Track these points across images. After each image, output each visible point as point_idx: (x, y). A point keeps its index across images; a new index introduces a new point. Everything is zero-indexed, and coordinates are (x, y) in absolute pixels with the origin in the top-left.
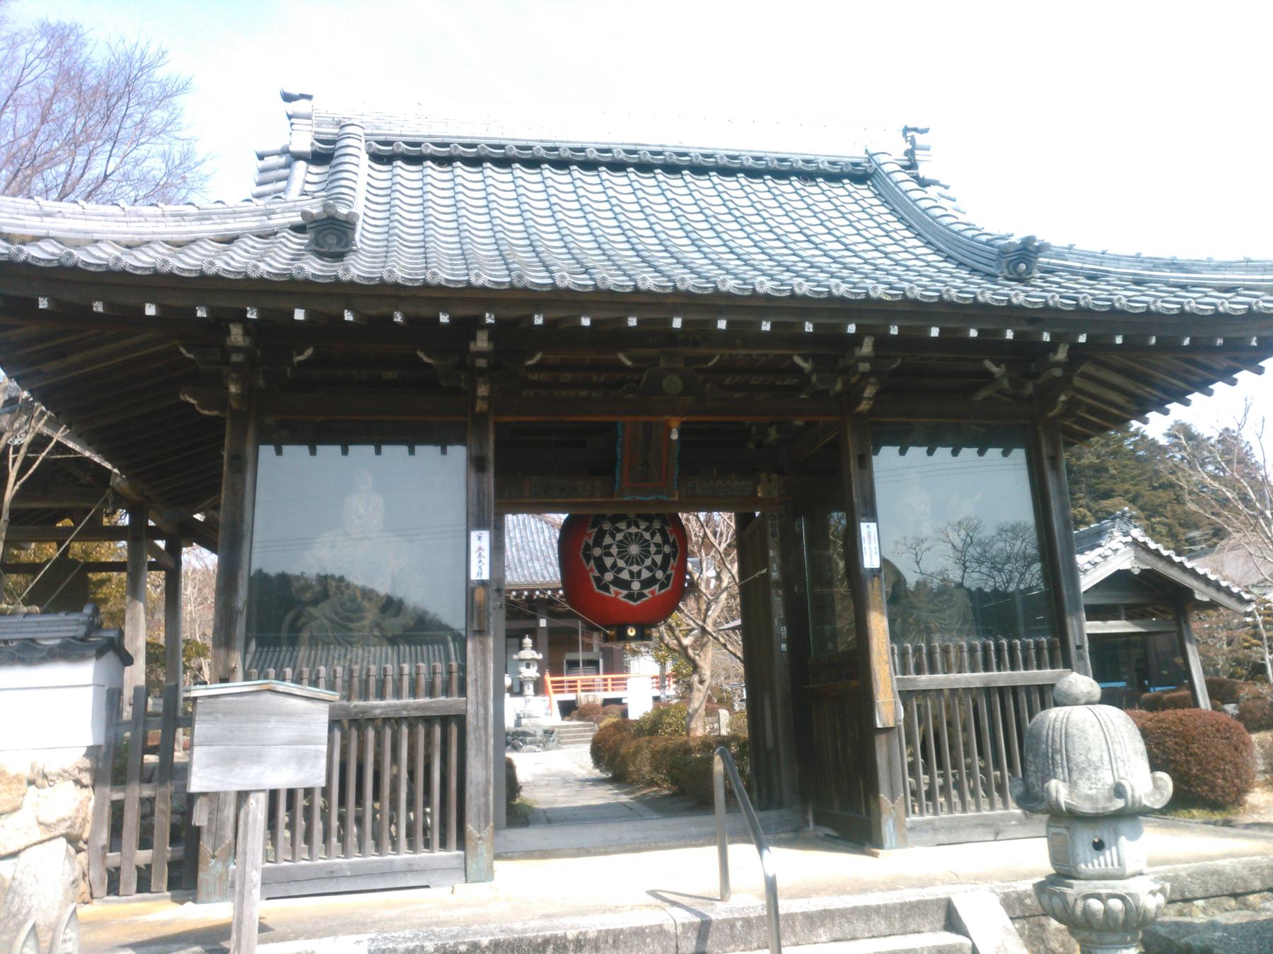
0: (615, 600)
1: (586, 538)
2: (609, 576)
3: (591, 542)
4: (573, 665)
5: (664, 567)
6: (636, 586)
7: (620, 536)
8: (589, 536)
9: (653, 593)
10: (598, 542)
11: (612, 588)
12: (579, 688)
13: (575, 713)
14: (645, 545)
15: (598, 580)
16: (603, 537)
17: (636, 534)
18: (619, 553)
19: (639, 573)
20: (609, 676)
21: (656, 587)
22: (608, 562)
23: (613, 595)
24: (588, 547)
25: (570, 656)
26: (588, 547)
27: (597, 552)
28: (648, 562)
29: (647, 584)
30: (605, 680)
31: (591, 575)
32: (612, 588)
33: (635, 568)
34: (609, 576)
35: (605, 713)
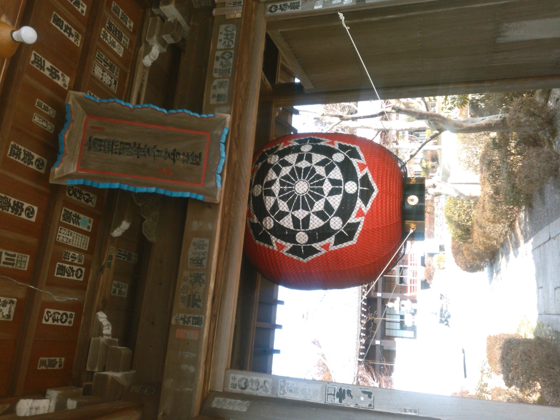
0: (369, 217)
1: (284, 251)
2: (336, 223)
3: (289, 246)
4: (402, 281)
5: (329, 152)
6: (351, 187)
7: (283, 206)
8: (281, 247)
9: (362, 167)
10: (290, 236)
11: (352, 219)
12: (415, 278)
13: (428, 281)
14: (297, 173)
15: (341, 238)
16: (283, 228)
17: (282, 184)
18: (305, 208)
19: (334, 182)
20: (409, 262)
21: (355, 162)
22: (316, 223)
23: (362, 219)
24: (295, 250)
25: (397, 282)
26: (295, 250)
27: (302, 238)
28: (321, 170)
29: (348, 172)
30: (411, 264)
31: (332, 248)
32: (352, 219)
33: (327, 187)
34: (336, 223)
35: (430, 265)
